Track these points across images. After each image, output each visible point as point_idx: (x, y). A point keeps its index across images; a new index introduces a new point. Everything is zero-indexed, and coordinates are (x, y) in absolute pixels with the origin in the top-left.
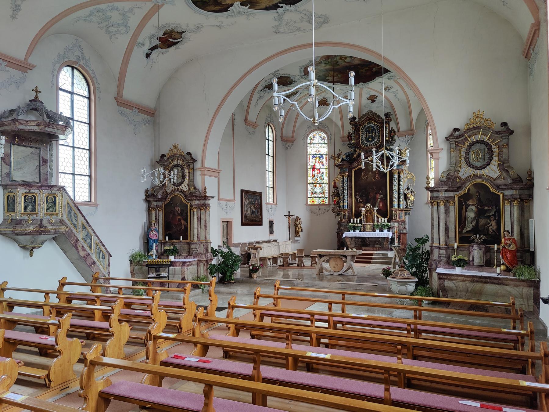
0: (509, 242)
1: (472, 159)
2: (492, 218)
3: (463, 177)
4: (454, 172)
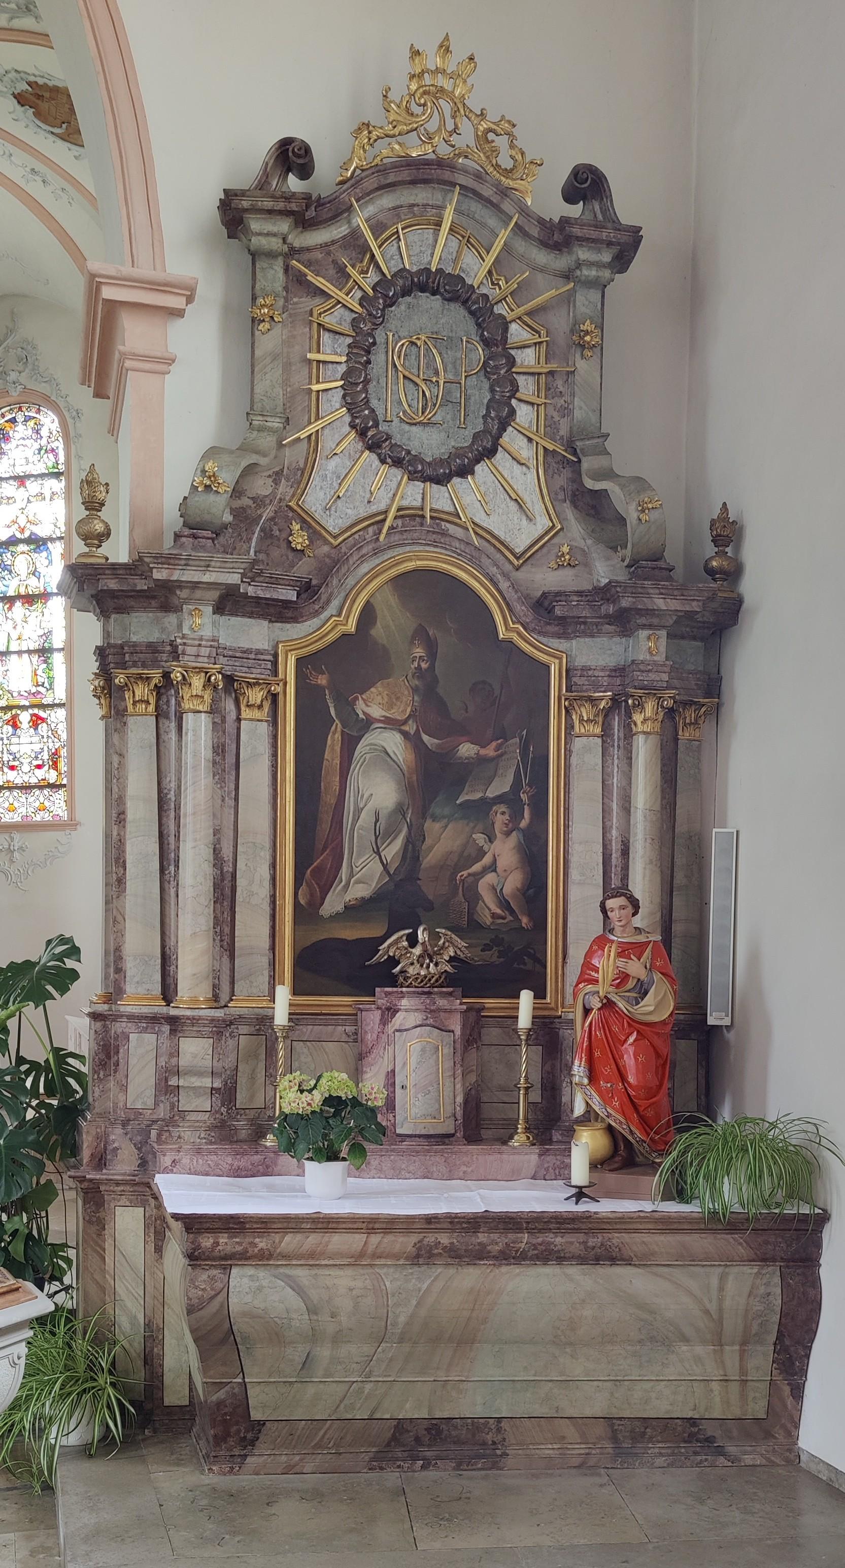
0: (636, 968)
1: (391, 400)
2: (500, 817)
4: (277, 477)
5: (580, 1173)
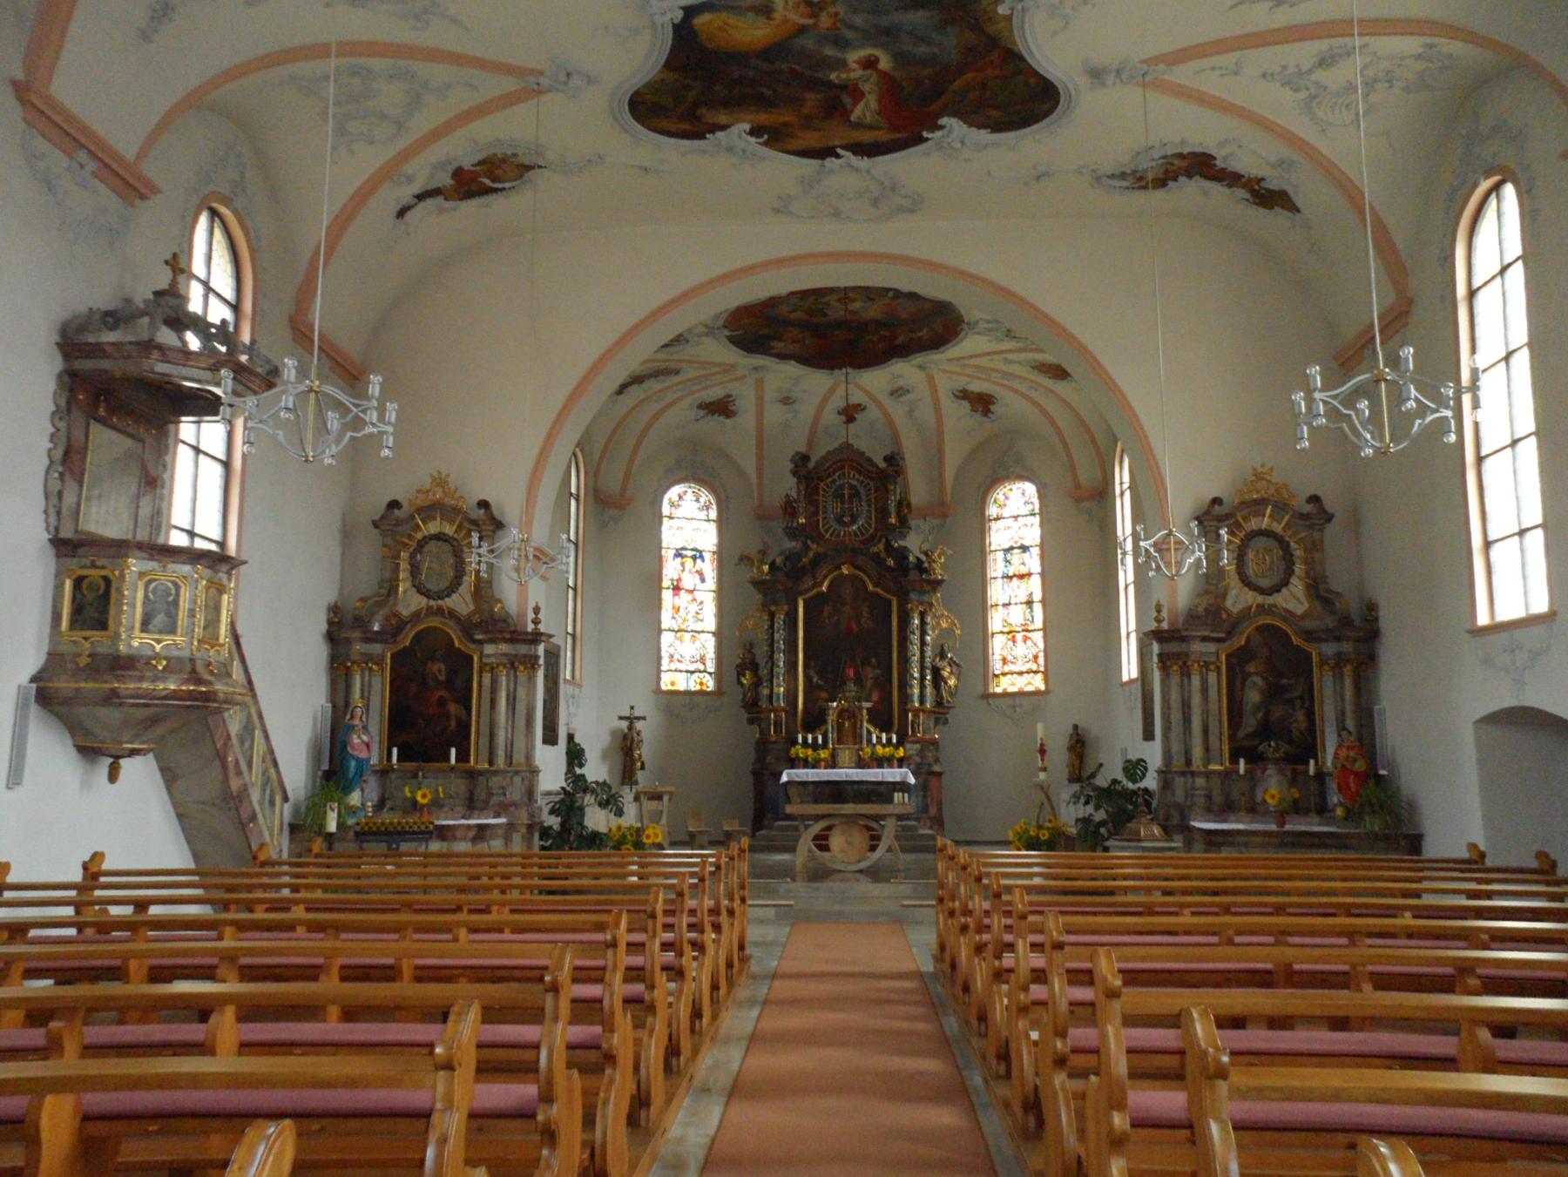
0: (1352, 754)
2: (1298, 703)
3: (1235, 610)
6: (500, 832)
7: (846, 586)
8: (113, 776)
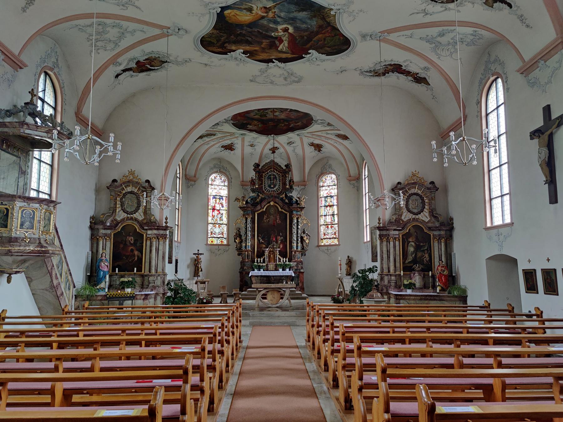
0: (443, 269)
2: (426, 252)
5: (438, 291)
6: (153, 296)
7: (271, 210)
8: (9, 281)
